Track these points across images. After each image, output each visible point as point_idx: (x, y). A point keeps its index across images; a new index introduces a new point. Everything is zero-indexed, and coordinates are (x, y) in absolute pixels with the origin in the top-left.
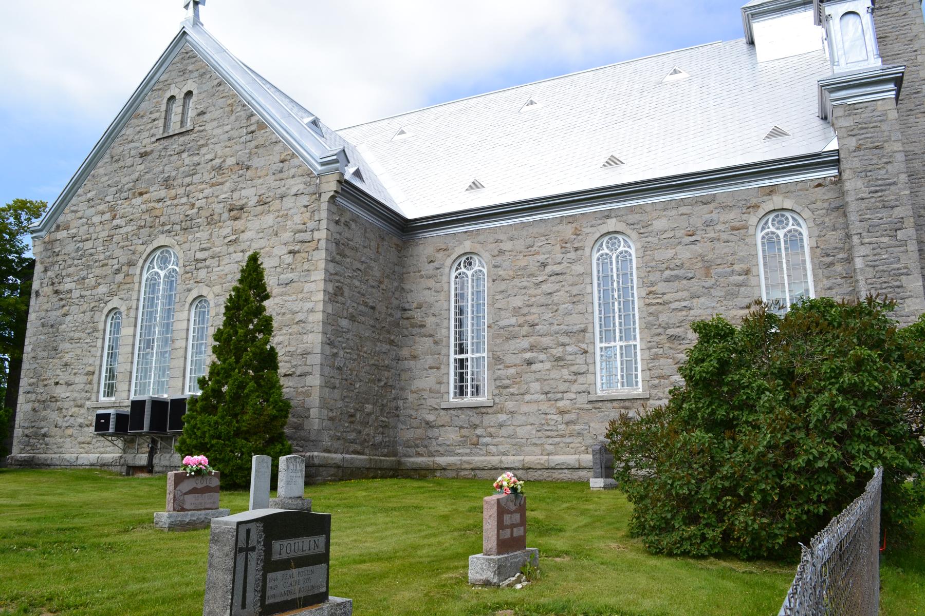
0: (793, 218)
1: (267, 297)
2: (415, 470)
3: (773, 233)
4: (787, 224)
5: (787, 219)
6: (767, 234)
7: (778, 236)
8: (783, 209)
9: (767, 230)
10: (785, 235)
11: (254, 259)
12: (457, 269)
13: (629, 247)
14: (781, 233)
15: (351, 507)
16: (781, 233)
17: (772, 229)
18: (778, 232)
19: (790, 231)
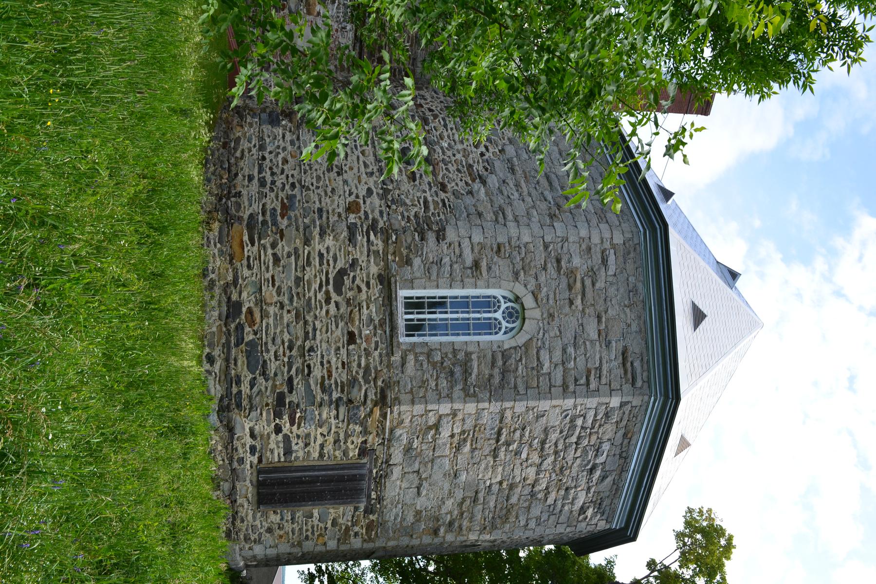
0: (513, 329)
1: (728, 558)
2: (328, 480)
3: (499, 307)
4: (507, 322)
5: (514, 322)
6: (499, 301)
7: (495, 311)
8: (524, 319)
9: (502, 300)
10: (496, 319)
11: (693, 304)
12: (504, 297)
13: (505, 333)
14: (498, 315)
15: (623, 354)
16: (498, 315)
17: (503, 306)
18: (501, 311)
19: (500, 323)
